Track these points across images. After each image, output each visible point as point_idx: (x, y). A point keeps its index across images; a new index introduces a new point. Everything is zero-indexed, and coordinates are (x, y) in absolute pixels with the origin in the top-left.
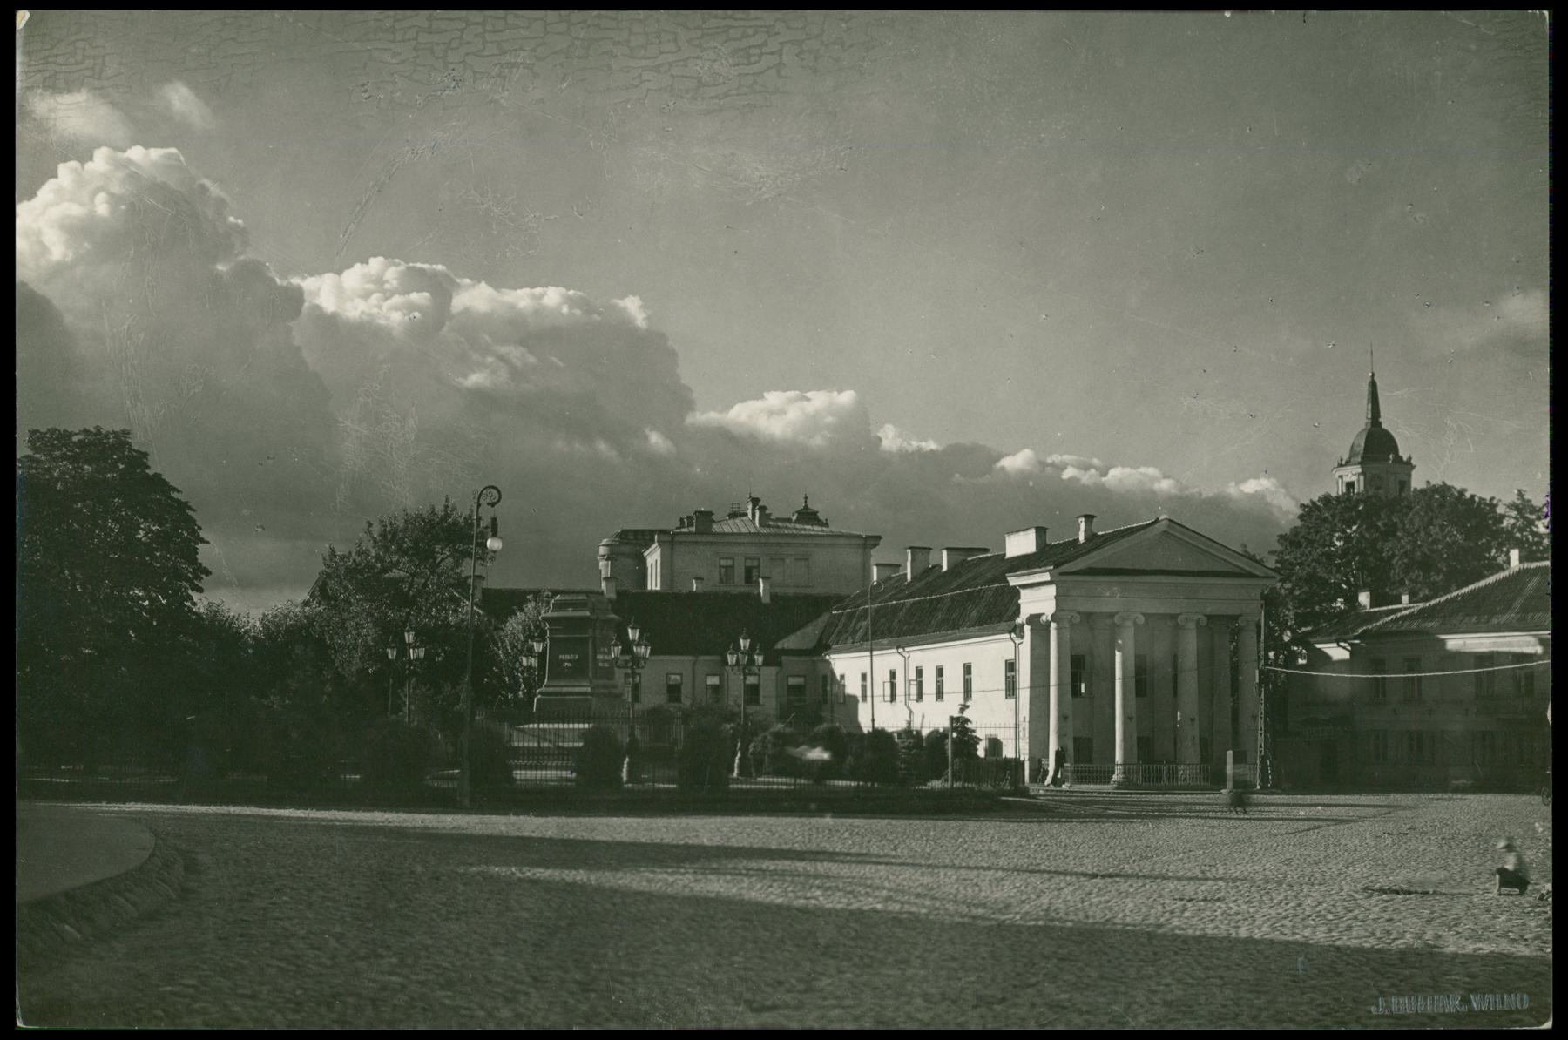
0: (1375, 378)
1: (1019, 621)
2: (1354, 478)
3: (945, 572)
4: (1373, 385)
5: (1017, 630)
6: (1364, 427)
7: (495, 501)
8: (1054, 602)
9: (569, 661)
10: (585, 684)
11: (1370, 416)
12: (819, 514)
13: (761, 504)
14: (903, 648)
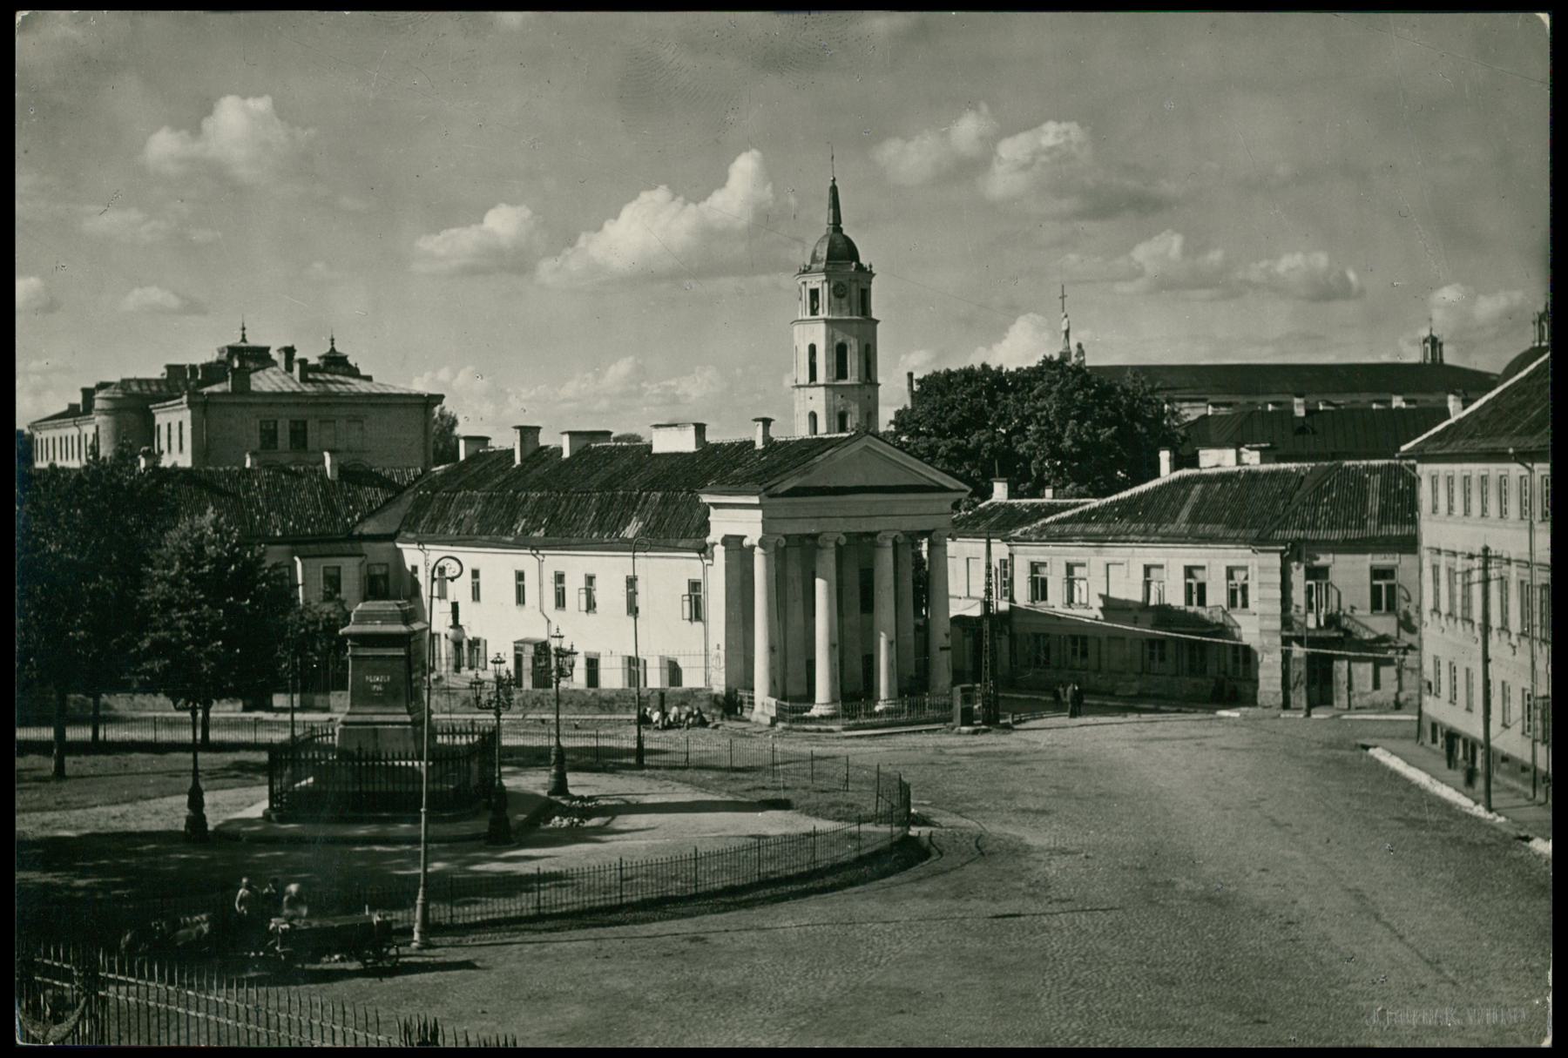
0: (836, 183)
1: (709, 540)
2: (818, 286)
3: (567, 460)
4: (834, 190)
5: (704, 550)
6: (825, 233)
7: (456, 574)
8: (760, 525)
9: (377, 683)
10: (400, 710)
11: (831, 222)
12: (348, 359)
13: (297, 356)
14: (537, 550)
